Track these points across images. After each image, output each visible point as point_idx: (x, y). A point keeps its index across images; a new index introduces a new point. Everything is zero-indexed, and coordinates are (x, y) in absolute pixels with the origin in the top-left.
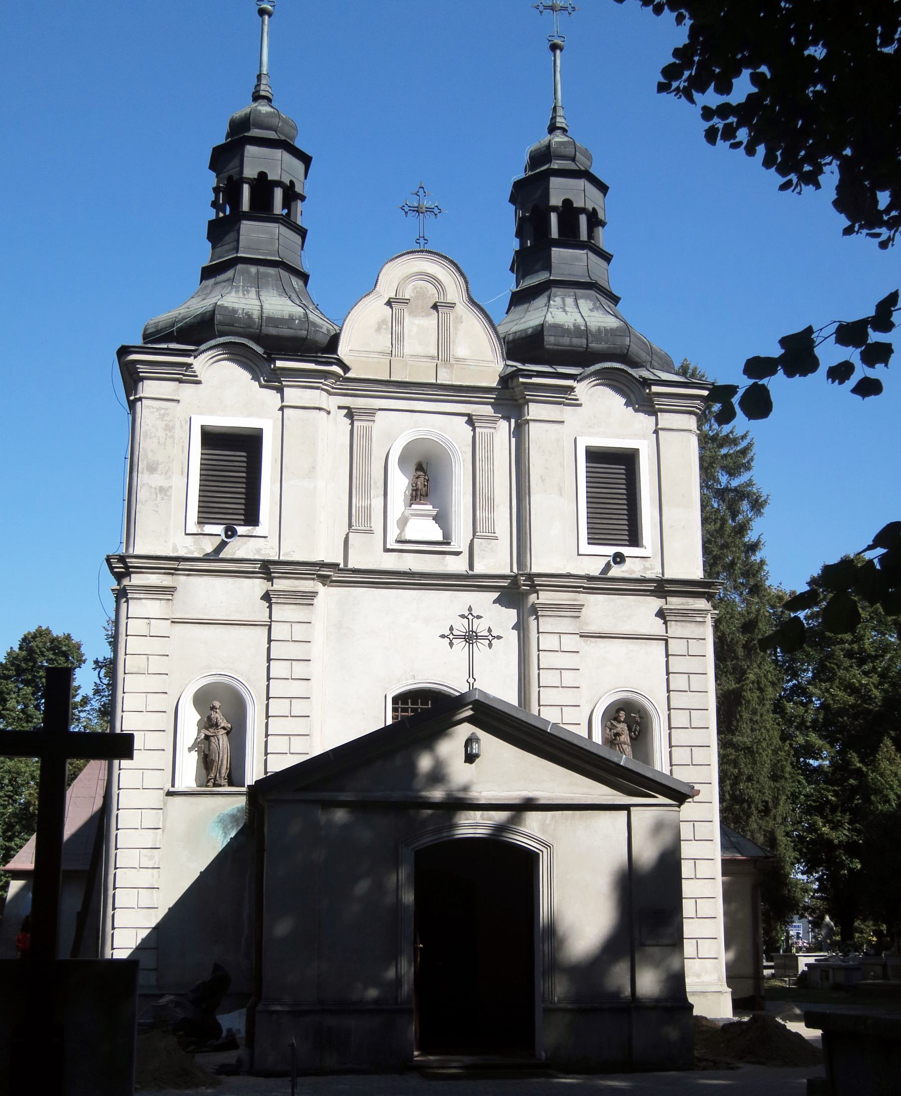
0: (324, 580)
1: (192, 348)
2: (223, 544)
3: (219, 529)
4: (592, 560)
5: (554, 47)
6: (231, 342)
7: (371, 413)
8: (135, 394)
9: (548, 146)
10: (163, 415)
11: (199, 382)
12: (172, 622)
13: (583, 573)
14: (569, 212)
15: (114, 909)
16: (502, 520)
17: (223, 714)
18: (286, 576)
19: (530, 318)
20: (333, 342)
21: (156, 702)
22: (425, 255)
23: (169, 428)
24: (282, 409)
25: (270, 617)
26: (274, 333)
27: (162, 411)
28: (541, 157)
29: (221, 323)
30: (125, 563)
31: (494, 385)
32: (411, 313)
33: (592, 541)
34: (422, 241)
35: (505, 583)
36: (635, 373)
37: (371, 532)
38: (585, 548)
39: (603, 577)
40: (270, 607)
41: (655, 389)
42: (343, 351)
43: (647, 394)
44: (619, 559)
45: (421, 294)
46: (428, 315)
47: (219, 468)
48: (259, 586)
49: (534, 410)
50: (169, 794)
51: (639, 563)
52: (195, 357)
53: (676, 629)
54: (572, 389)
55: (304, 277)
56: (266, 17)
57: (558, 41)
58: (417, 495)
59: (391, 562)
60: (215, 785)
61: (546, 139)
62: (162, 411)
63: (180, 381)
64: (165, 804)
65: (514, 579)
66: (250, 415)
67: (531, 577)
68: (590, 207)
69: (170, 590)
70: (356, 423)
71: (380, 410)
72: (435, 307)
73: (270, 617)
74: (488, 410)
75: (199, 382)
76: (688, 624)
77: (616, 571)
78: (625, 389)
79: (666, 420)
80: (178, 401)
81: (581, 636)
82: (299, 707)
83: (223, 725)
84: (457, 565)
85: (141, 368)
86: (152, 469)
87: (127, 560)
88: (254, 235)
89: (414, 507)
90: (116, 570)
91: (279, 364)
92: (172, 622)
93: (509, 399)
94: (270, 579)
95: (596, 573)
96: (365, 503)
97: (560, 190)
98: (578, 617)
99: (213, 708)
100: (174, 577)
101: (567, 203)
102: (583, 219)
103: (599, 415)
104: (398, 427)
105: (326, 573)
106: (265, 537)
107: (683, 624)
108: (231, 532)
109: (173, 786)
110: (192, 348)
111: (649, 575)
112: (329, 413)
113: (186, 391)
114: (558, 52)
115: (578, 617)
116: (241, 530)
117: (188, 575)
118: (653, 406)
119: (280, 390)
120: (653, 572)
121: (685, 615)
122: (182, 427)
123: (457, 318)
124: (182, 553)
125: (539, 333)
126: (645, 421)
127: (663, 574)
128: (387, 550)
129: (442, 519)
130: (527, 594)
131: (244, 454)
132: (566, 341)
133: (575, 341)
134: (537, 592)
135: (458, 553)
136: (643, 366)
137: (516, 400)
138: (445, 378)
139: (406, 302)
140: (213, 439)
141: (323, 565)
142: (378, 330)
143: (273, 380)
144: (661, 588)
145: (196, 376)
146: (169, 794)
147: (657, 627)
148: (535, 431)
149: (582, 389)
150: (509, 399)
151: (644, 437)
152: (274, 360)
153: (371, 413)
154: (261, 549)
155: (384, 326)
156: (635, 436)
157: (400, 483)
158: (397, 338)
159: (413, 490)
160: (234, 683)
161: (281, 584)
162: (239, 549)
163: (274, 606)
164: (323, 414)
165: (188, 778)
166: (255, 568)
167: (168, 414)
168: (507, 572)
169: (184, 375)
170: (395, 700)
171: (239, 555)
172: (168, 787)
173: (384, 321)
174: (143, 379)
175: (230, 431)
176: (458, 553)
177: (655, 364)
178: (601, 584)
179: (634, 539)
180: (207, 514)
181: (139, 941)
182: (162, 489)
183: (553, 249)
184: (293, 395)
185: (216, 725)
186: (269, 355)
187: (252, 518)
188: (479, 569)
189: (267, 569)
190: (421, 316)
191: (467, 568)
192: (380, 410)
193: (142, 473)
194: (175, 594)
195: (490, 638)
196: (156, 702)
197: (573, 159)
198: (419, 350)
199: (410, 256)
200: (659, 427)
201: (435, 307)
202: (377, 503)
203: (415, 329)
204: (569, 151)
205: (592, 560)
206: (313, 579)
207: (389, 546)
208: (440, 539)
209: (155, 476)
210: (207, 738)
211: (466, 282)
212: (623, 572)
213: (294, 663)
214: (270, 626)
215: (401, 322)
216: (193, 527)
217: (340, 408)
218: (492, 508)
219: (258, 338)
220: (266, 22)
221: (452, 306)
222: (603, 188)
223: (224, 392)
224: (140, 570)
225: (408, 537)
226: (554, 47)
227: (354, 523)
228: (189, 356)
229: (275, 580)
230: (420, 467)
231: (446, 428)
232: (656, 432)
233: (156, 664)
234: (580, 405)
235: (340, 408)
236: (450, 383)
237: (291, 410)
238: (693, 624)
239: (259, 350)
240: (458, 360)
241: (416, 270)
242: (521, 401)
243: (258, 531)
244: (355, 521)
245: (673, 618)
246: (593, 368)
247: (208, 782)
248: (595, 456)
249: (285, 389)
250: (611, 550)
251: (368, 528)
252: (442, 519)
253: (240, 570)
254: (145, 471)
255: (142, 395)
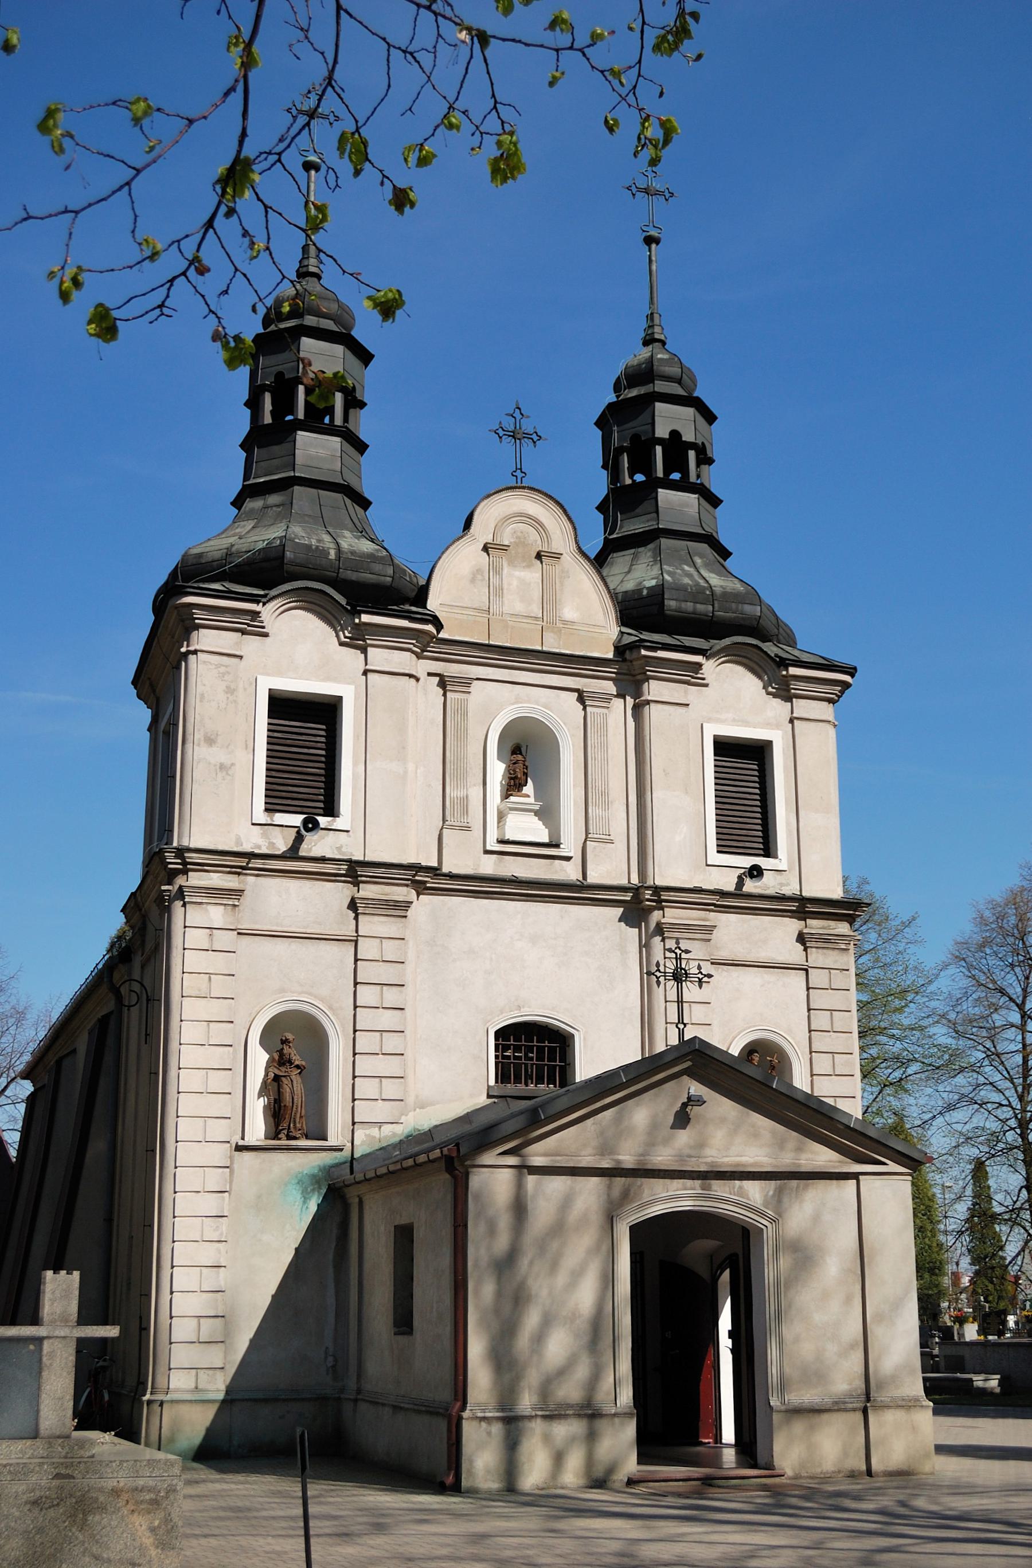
0: (421, 889)
1: (262, 593)
2: (299, 839)
3: (297, 820)
4: (723, 871)
5: (649, 240)
6: (307, 588)
7: (466, 682)
8: (188, 646)
9: (650, 361)
10: (224, 674)
11: (266, 635)
12: (239, 934)
13: (712, 888)
14: (675, 445)
15: (172, 1293)
16: (618, 820)
17: (295, 1051)
18: (374, 880)
19: (640, 573)
20: (421, 595)
21: (220, 1033)
22: (518, 492)
23: (230, 691)
24: (365, 673)
25: (357, 931)
26: (354, 578)
27: (222, 669)
28: (640, 375)
29: (292, 563)
30: (183, 858)
31: (610, 655)
32: (511, 563)
33: (722, 849)
34: (518, 473)
35: (628, 897)
36: (771, 649)
37: (467, 828)
38: (715, 858)
39: (738, 893)
40: (356, 918)
41: (793, 671)
42: (434, 603)
43: (784, 676)
44: (756, 872)
45: (521, 542)
46: (529, 566)
47: (289, 742)
48: (342, 892)
49: (655, 689)
50: (239, 1148)
51: (780, 875)
52: (264, 604)
53: (817, 958)
54: (699, 665)
55: (365, 504)
56: (313, 172)
57: (654, 233)
58: (514, 785)
59: (489, 866)
60: (289, 1137)
61: (645, 353)
62: (222, 669)
63: (243, 632)
64: (231, 1158)
65: (636, 891)
66: (328, 679)
67: (657, 890)
68: (699, 442)
69: (238, 893)
70: (449, 694)
71: (478, 679)
72: (539, 556)
73: (357, 931)
74: (610, 687)
75: (266, 635)
76: (830, 952)
77: (751, 886)
78: (756, 667)
79: (802, 708)
80: (241, 657)
81: (712, 963)
82: (391, 1043)
83: (297, 1063)
84: (570, 872)
85: (198, 613)
86: (210, 741)
87: (186, 855)
88: (312, 451)
89: (512, 799)
90: (170, 866)
91: (365, 618)
92: (239, 934)
93: (629, 671)
94: (356, 884)
95: (731, 887)
96: (461, 793)
97: (669, 419)
98: (709, 940)
99: (285, 1042)
100: (242, 877)
101: (675, 434)
102: (692, 454)
103: (731, 699)
104: (500, 700)
105: (426, 879)
106: (348, 831)
107: (825, 951)
108: (311, 825)
109: (243, 1138)
110: (262, 593)
111: (787, 891)
112: (418, 680)
113: (250, 645)
114: (654, 246)
115: (709, 940)
116: (323, 821)
117: (257, 875)
118: (789, 691)
119: (364, 650)
120: (791, 889)
121: (827, 941)
122: (245, 689)
123: (563, 571)
124: (247, 848)
125: (658, 593)
126: (779, 708)
127: (801, 891)
128: (487, 852)
129: (547, 813)
130: (650, 910)
131: (324, 727)
132: (689, 606)
133: (701, 608)
134: (662, 908)
135: (568, 859)
136: (770, 641)
137: (634, 676)
138: (552, 644)
139: (504, 548)
140: (282, 706)
141: (417, 868)
142: (473, 580)
143: (359, 640)
144: (803, 907)
145: (263, 627)
146: (239, 1148)
147: (794, 953)
148: (655, 714)
149: (710, 668)
150: (629, 671)
151: (778, 726)
152: (360, 613)
153: (466, 682)
154: (341, 846)
155: (479, 577)
156: (768, 725)
157: (497, 770)
158: (496, 592)
159: (511, 779)
160: (313, 1011)
161: (368, 891)
162: (316, 845)
163: (360, 917)
164: (413, 680)
165: (257, 1130)
166: (339, 869)
167: (229, 673)
168: (624, 882)
169: (249, 625)
170: (499, 1034)
171: (316, 852)
172: (236, 1139)
173: (479, 571)
174: (198, 627)
175: (294, 696)
176: (568, 859)
177: (781, 637)
178: (733, 901)
179: (768, 850)
180: (275, 801)
181: (830, 1101)
182: (222, 767)
183: (660, 490)
184: (378, 657)
185: (290, 1062)
186: (354, 607)
187: (331, 809)
188: (593, 878)
189: (354, 871)
190: (523, 568)
191: (581, 879)
192: (478, 679)
193: (199, 745)
194: (242, 899)
195: (677, 951)
196: (220, 1033)
197: (679, 381)
198: (519, 607)
199: (510, 493)
200: (795, 715)
201: (539, 556)
202: (475, 794)
203: (515, 583)
204: (675, 371)
205: (723, 871)
206: (407, 885)
207: (489, 848)
208: (546, 840)
209: (214, 749)
210: (277, 1078)
211: (575, 529)
212: (756, 887)
213: (385, 988)
214: (356, 942)
215: (498, 572)
216: (261, 817)
217: (430, 674)
218: (607, 805)
219: (336, 583)
220: (313, 179)
221: (557, 556)
222: (710, 417)
223: (297, 649)
224: (201, 868)
225: (510, 836)
226: (649, 240)
227: (448, 818)
228: (258, 602)
229: (361, 885)
230: (517, 750)
231: (552, 705)
232: (791, 721)
233: (219, 986)
234: (706, 685)
235: (430, 674)
236: (557, 651)
237: (376, 675)
238: (836, 952)
239: (343, 601)
240: (565, 622)
241: (515, 509)
242: (639, 677)
243: (339, 823)
244: (450, 817)
245: (813, 944)
246: (727, 641)
247: (279, 1133)
248: (724, 747)
249: (369, 649)
250: (747, 862)
251: (465, 824)
252: (547, 813)
253: (323, 869)
254: (202, 743)
255: (198, 647)
